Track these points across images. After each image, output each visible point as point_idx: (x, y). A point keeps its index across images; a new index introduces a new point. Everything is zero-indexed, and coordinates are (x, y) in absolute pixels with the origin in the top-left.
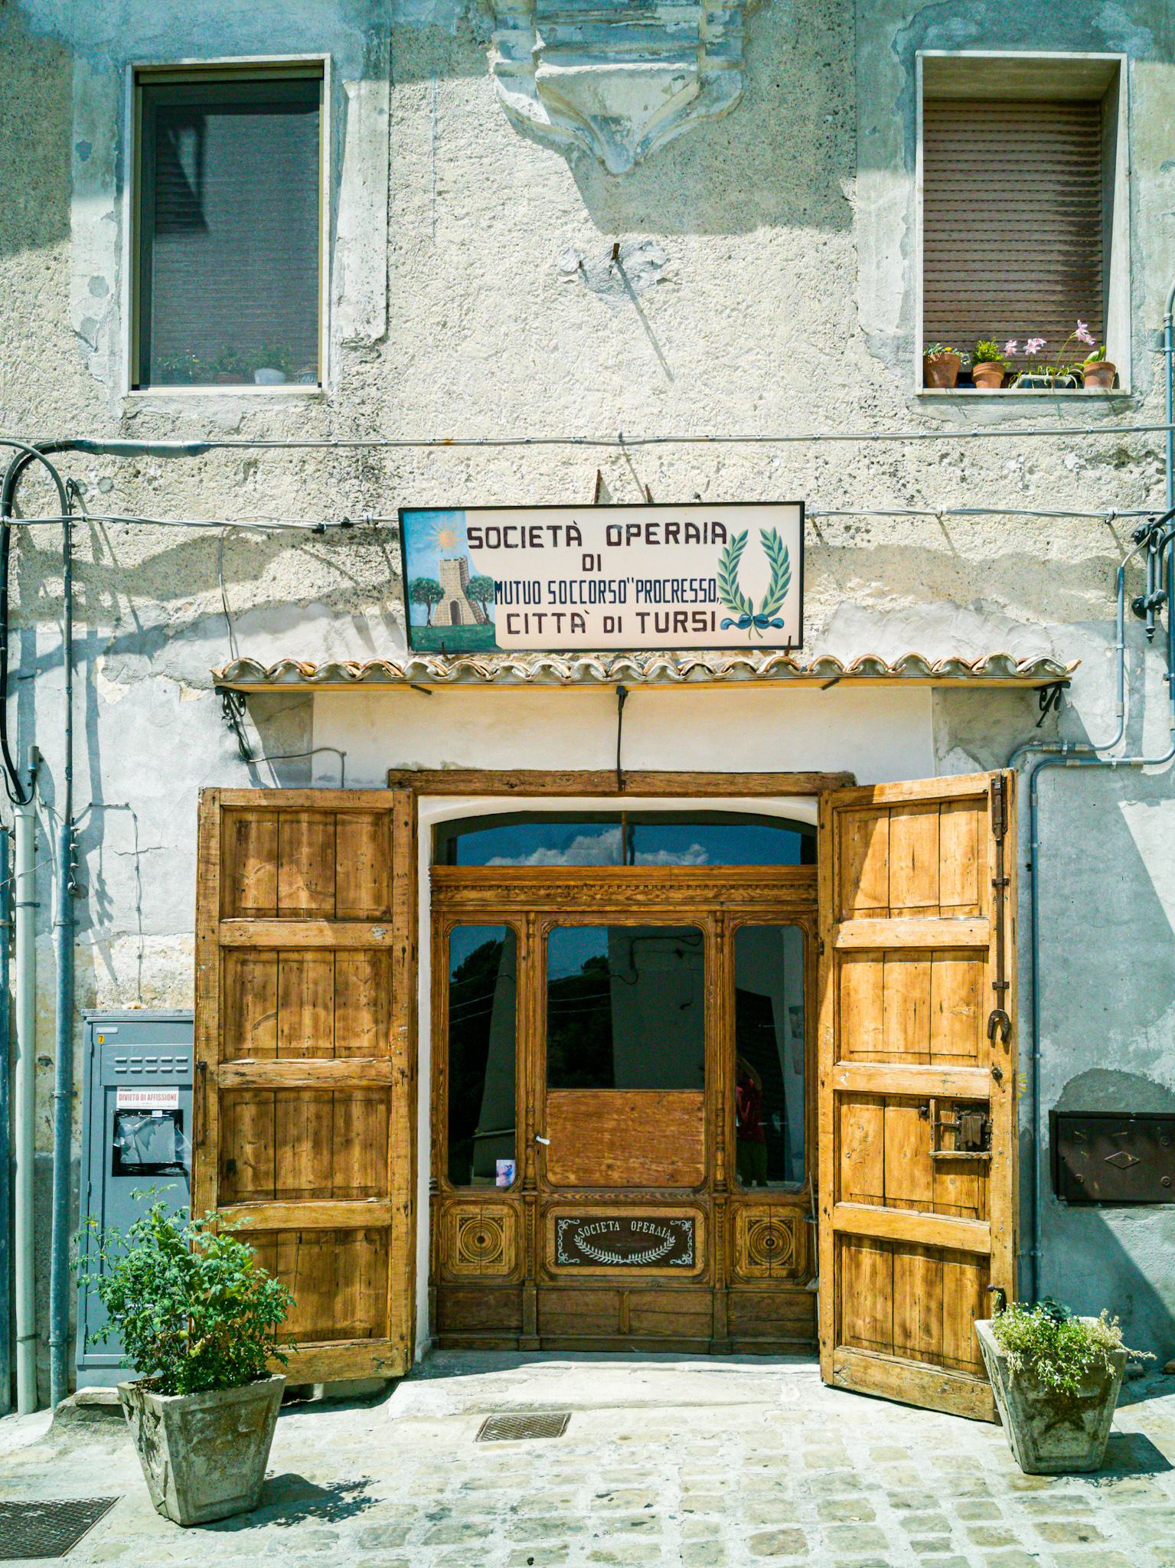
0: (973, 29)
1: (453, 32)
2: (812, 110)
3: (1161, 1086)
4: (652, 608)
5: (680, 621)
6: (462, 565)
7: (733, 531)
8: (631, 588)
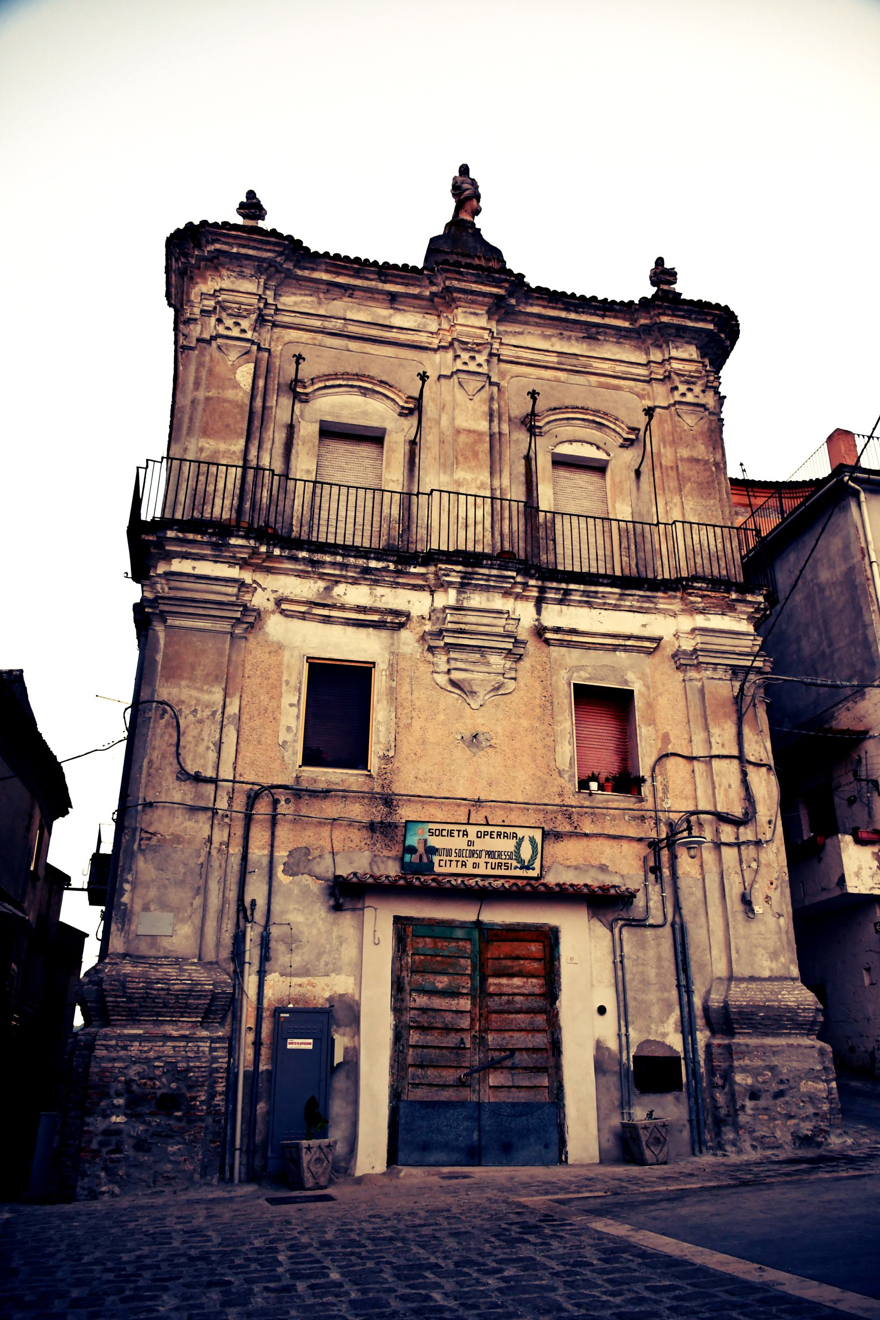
0: (588, 676)
1: (418, 657)
2: (538, 695)
3: (669, 1046)
4: (490, 860)
5: (500, 866)
6: (426, 841)
7: (520, 836)
8: (484, 853)
